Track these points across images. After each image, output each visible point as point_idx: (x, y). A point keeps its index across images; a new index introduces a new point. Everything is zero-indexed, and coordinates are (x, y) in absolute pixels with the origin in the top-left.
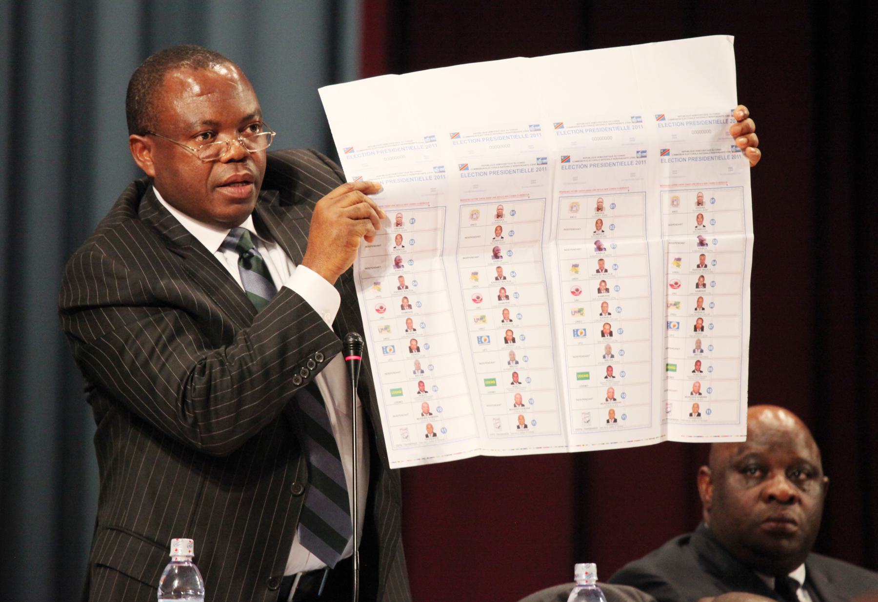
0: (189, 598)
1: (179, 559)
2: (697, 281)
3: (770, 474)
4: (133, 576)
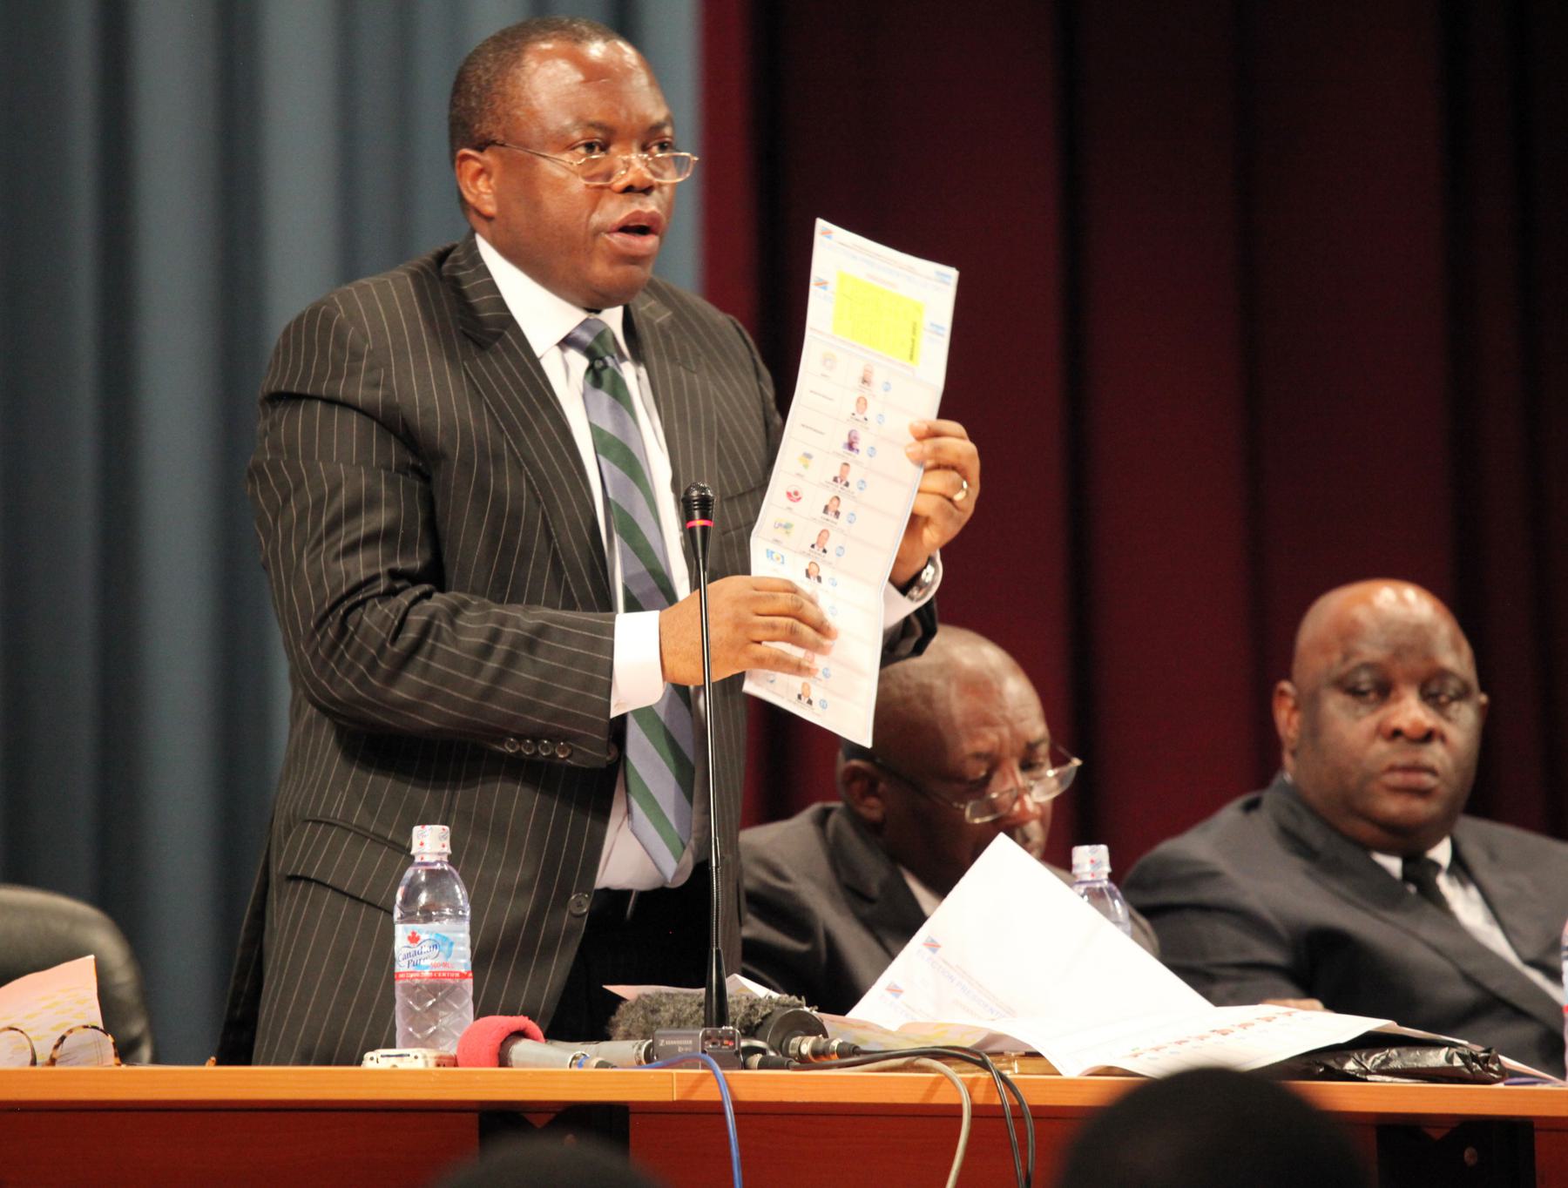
0: (446, 922)
1: (427, 859)
2: (827, 502)
3: (1393, 695)
4: (320, 878)
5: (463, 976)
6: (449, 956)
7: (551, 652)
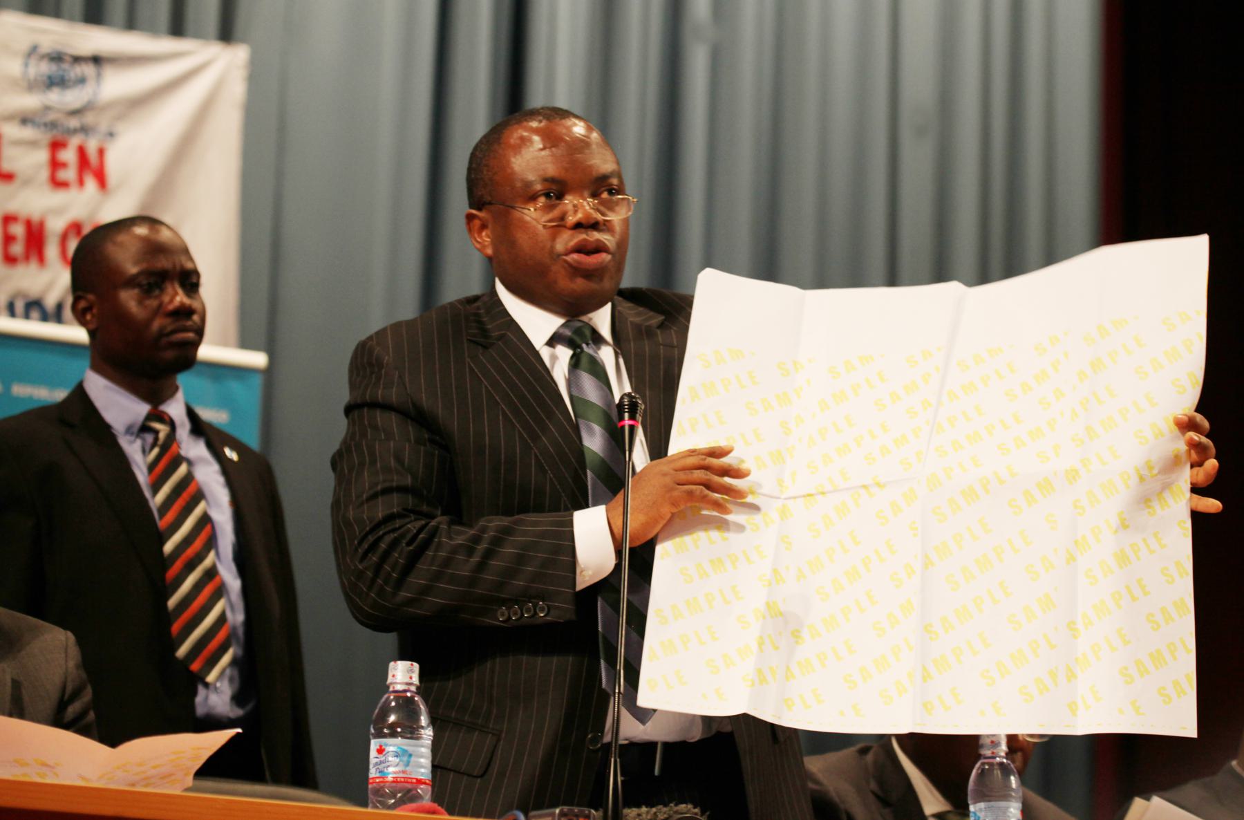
5: (419, 782)
6: (407, 764)
7: (525, 533)
